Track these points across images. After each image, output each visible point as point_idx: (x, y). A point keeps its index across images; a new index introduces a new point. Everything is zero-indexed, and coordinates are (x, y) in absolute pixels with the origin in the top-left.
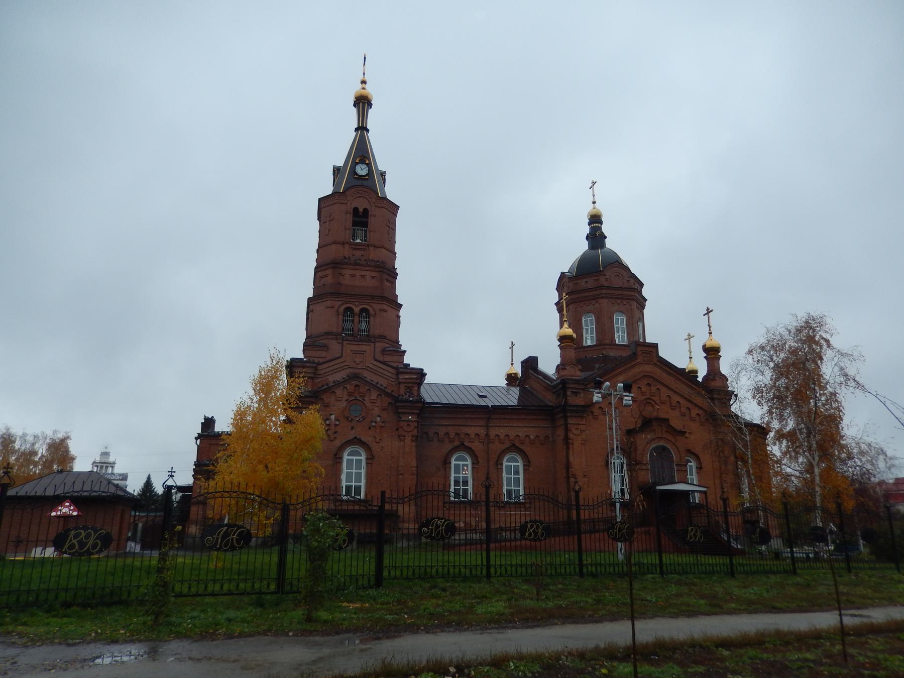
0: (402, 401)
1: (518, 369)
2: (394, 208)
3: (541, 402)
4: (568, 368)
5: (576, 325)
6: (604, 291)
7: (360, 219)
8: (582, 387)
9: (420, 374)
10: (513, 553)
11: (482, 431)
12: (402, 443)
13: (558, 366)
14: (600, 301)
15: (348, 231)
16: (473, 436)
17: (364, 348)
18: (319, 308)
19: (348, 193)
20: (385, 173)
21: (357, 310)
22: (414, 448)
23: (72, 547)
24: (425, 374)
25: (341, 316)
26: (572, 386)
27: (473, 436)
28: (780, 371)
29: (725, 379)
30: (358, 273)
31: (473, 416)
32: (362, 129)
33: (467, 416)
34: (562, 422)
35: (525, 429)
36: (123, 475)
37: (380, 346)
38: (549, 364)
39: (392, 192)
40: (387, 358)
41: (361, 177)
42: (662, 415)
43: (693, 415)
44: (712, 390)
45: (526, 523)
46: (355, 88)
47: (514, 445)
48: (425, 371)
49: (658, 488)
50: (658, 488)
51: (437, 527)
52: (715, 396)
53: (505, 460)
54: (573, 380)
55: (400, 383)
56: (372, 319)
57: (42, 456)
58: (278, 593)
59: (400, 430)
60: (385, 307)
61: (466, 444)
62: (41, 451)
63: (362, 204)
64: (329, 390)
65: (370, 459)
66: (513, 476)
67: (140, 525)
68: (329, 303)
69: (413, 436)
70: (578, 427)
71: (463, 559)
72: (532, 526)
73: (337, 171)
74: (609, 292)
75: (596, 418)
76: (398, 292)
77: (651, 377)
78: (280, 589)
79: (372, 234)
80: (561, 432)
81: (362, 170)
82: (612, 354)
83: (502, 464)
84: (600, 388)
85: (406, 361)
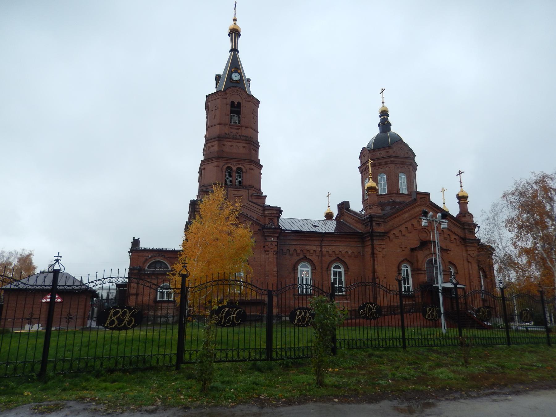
0: (267, 228)
3: (351, 230)
4: (373, 208)
6: (392, 159)
7: (236, 108)
8: (382, 220)
10: (358, 328)
11: (318, 249)
12: (267, 256)
14: (390, 165)
15: (227, 117)
16: (312, 252)
17: (241, 193)
18: (210, 167)
19: (227, 92)
20: (250, 80)
21: (234, 168)
22: (275, 260)
23: (112, 322)
24: (282, 211)
25: (224, 173)
26: (376, 219)
27: (312, 252)
28: (525, 207)
29: (471, 216)
31: (311, 239)
32: (234, 50)
33: (308, 239)
34: (370, 243)
35: (346, 247)
38: (357, 206)
39: (255, 91)
40: (255, 200)
43: (452, 239)
44: (464, 223)
46: (230, 24)
48: (282, 209)
52: (466, 227)
54: (376, 215)
55: (265, 216)
56: (244, 174)
57: (15, 266)
58: (268, 360)
59: (266, 247)
60: (252, 167)
61: (308, 257)
62: (14, 263)
67: (96, 309)
68: (216, 164)
69: (274, 251)
70: (381, 246)
71: (394, 333)
73: (218, 77)
74: (396, 160)
75: (391, 240)
78: (269, 357)
80: (369, 250)
81: (235, 77)
83: (331, 270)
84: (426, 216)
85: (268, 202)
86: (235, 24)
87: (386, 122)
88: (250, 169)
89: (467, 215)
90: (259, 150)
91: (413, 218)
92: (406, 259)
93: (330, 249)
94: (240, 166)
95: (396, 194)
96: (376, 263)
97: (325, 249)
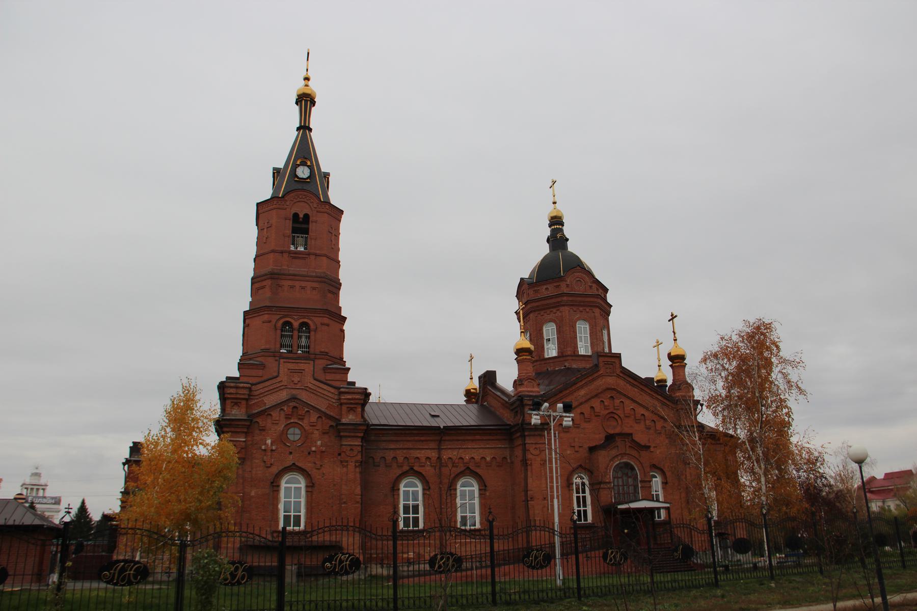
1: (476, 384)
2: (337, 213)
3: (498, 419)
4: (526, 383)
5: (536, 336)
6: (565, 298)
7: (301, 225)
9: (365, 394)
11: (434, 455)
13: (515, 381)
14: (562, 308)
16: (423, 460)
17: (302, 366)
18: (257, 322)
20: (328, 174)
21: (296, 324)
22: (358, 475)
24: (370, 394)
25: (279, 332)
30: (297, 284)
32: (304, 128)
35: (481, 450)
36: (55, 498)
37: (321, 363)
38: (507, 378)
39: (336, 197)
41: (302, 181)
42: (627, 430)
45: (436, 555)
46: (298, 86)
47: (468, 468)
48: (369, 391)
49: (619, 507)
50: (619, 507)
51: (341, 561)
53: (458, 486)
55: (341, 404)
56: (312, 333)
59: (343, 455)
63: (302, 210)
64: (265, 413)
65: (310, 487)
66: (468, 502)
68: (266, 317)
70: (538, 446)
72: (442, 558)
73: (277, 172)
74: (571, 299)
76: (341, 304)
77: (614, 389)
79: (313, 242)
82: (574, 366)
83: (456, 489)
85: (351, 377)
86: (307, 86)
87: (559, 236)
88: (322, 324)
89: (683, 387)
90: (341, 292)
91: (593, 397)
92: (581, 466)
93: (454, 454)
94: (306, 320)
95: (571, 356)
96: (529, 473)
97: (445, 456)
